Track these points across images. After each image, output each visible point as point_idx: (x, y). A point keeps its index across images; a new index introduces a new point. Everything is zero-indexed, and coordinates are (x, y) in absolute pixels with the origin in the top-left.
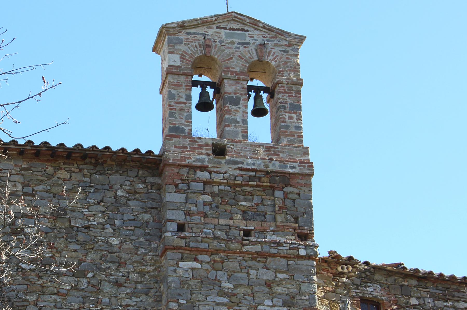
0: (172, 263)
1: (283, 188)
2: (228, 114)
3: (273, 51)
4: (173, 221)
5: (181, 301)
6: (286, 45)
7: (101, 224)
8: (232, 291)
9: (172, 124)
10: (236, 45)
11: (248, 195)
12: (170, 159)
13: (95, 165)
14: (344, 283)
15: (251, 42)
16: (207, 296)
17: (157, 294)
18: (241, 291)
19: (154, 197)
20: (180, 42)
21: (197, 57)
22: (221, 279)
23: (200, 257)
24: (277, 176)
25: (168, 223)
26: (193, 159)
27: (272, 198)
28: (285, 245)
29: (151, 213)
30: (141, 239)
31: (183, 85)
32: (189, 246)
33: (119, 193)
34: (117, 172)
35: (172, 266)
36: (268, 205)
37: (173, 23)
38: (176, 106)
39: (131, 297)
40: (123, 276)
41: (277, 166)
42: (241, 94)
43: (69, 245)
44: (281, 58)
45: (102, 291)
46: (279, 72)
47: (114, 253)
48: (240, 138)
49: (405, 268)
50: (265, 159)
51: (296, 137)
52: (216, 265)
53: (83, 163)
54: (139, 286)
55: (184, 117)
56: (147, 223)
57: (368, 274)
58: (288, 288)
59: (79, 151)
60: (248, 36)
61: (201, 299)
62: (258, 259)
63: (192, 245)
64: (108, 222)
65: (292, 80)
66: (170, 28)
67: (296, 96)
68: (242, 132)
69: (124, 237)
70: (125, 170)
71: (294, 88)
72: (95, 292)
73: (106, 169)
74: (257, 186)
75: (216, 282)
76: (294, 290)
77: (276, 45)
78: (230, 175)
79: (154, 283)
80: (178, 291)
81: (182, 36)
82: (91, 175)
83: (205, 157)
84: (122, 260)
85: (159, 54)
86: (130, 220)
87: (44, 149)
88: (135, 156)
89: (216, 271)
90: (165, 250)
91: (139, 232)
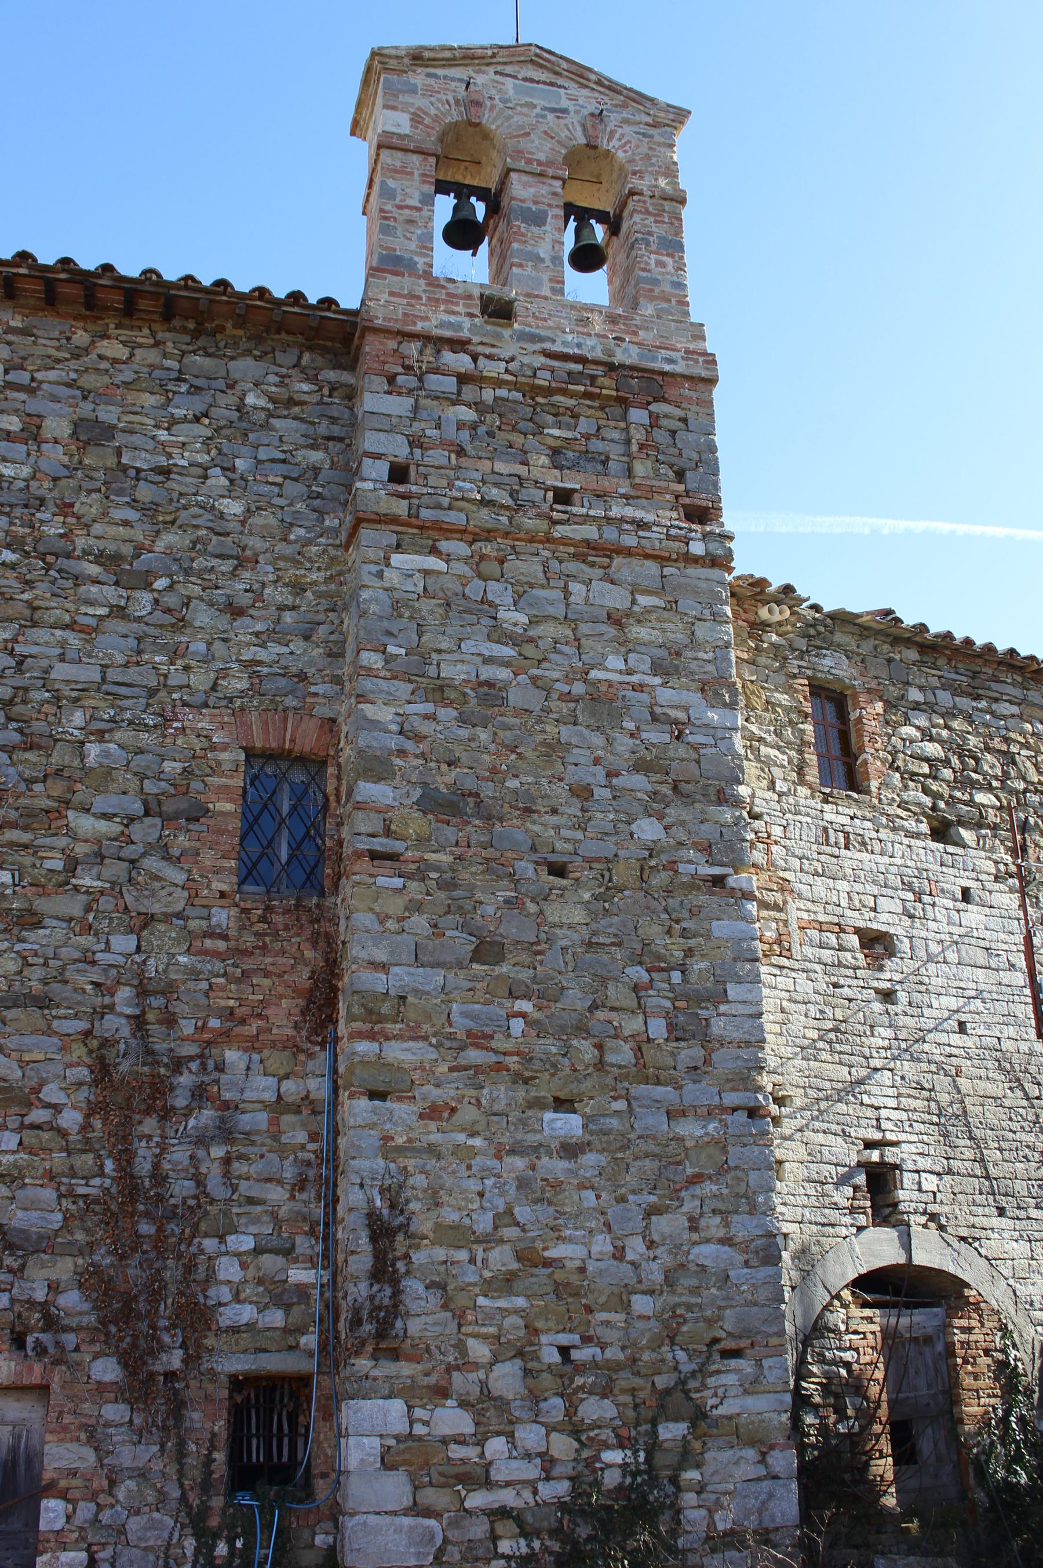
0: (371, 554)
1: (649, 403)
2: (519, 241)
3: (620, 131)
4: (378, 456)
5: (391, 649)
6: (647, 124)
7: (200, 465)
8: (525, 630)
9: (387, 248)
10: (538, 110)
11: (564, 415)
12: (377, 318)
13: (196, 334)
14: (772, 644)
15: (572, 109)
16: (461, 640)
17: (332, 638)
18: (548, 631)
19: (336, 414)
20: (413, 91)
21: (450, 123)
22: (497, 601)
23: (444, 545)
24: (633, 378)
25: (367, 461)
26: (434, 322)
27: (622, 425)
28: (655, 528)
29: (326, 449)
30: (300, 506)
31: (416, 173)
32: (417, 517)
33: (250, 400)
34: (248, 352)
35: (371, 562)
36: (612, 441)
37: (396, 48)
38: (396, 213)
39: (265, 642)
40: (246, 591)
41: (634, 355)
42: (549, 205)
43: (111, 510)
44: (637, 147)
45: (192, 626)
46: (634, 173)
47: (228, 534)
48: (546, 291)
49: (898, 620)
50: (605, 337)
51: (674, 303)
52: (486, 567)
53: (165, 327)
54: (288, 617)
55: (414, 237)
56: (316, 470)
57: (822, 629)
58: (664, 631)
59: (151, 289)
60: (564, 97)
61: (444, 646)
62: (590, 559)
63: (425, 514)
64: (218, 461)
65: (663, 190)
66: (390, 57)
67: (672, 224)
68: (551, 280)
69: (256, 498)
70: (269, 349)
71: (667, 205)
72: (173, 625)
73: (222, 344)
74: (587, 395)
75: (486, 607)
76: (680, 636)
77: (626, 121)
78: (522, 365)
79: (326, 610)
80: (386, 624)
81: (418, 78)
82: (182, 356)
83: (465, 323)
84: (248, 553)
85: (365, 139)
86: (273, 461)
87: (63, 276)
88: (291, 309)
89: (485, 580)
90: (358, 523)
91: (293, 489)
